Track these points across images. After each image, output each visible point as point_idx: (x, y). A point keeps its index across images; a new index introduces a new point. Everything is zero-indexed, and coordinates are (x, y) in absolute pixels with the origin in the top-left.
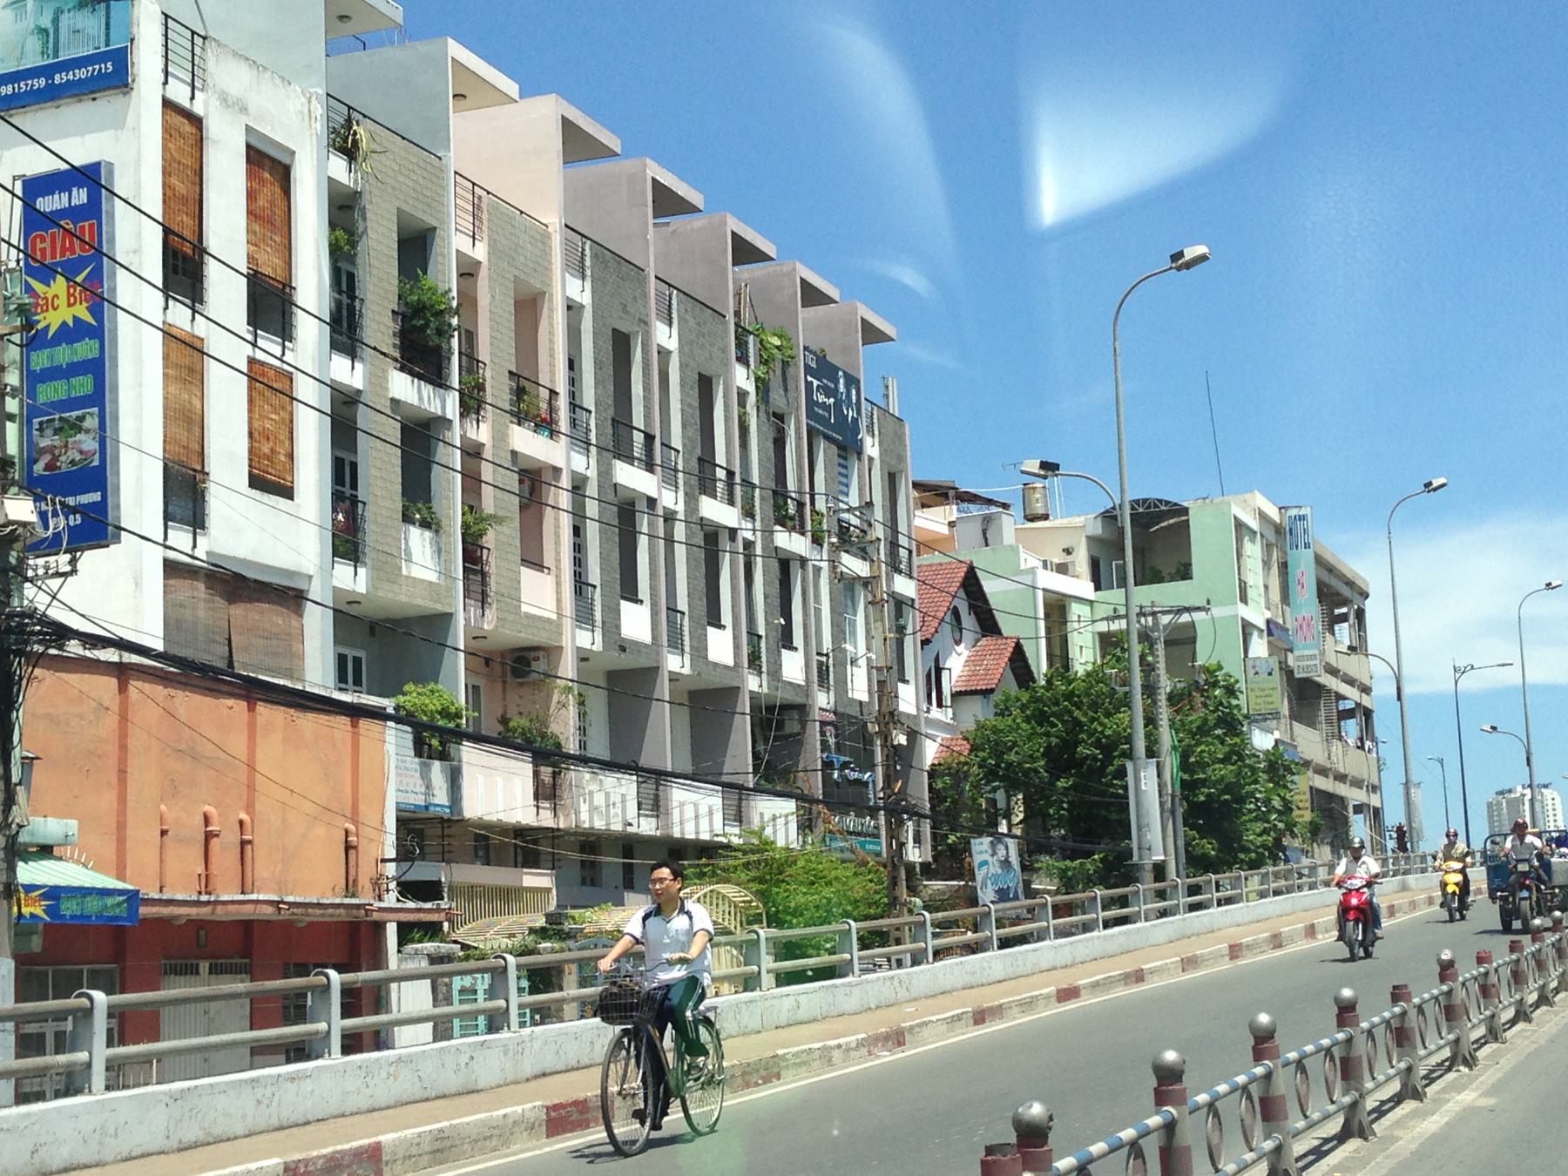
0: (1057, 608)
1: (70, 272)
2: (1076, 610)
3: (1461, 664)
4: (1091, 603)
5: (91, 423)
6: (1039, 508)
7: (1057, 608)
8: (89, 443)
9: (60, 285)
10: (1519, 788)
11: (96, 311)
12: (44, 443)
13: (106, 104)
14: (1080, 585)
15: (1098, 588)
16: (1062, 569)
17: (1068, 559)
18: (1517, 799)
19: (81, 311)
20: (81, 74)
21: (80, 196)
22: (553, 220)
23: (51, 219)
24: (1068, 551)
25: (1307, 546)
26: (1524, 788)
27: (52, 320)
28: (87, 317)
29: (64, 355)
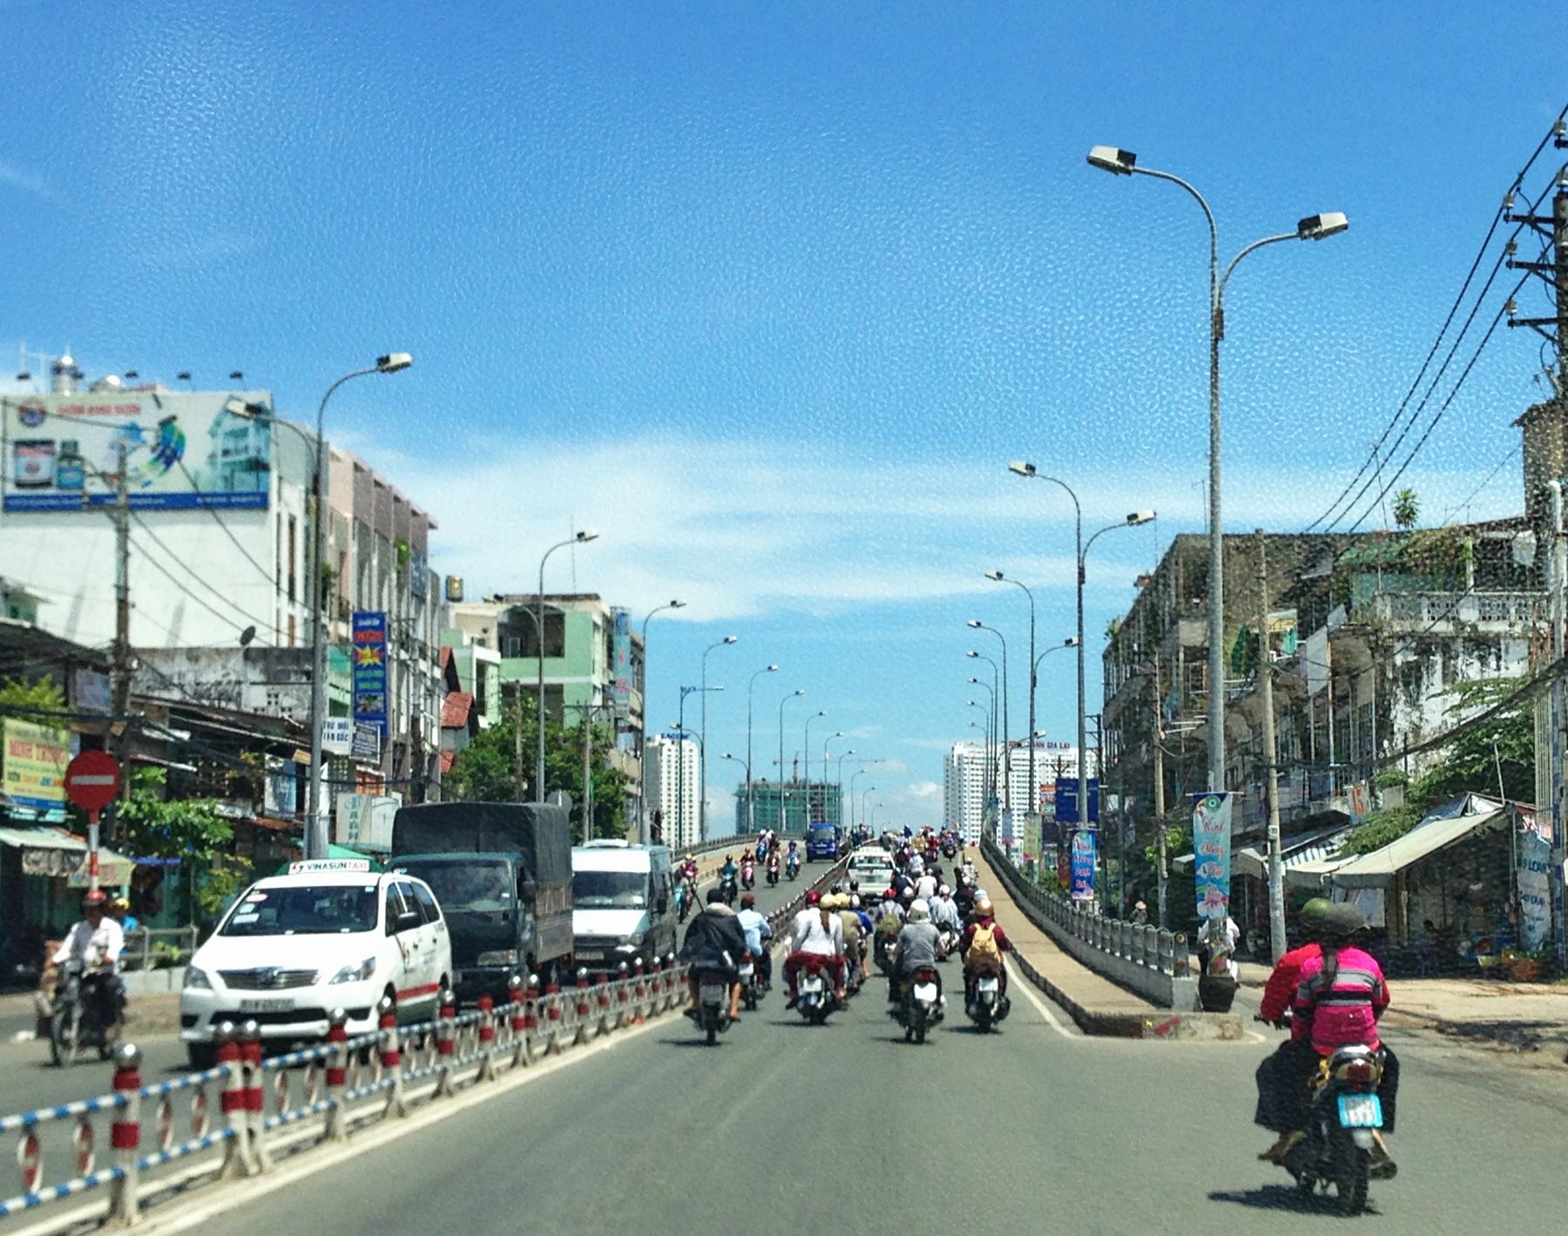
0: (482, 667)
1: (372, 646)
2: (491, 671)
3: (686, 685)
4: (498, 666)
5: (381, 698)
6: (457, 594)
7: (482, 667)
8: (380, 705)
9: (367, 650)
10: (658, 738)
11: (383, 661)
12: (362, 702)
13: (255, 515)
14: (491, 654)
15: (502, 657)
16: (482, 643)
17: (485, 636)
18: (655, 749)
19: (377, 661)
20: (244, 500)
21: (376, 622)
22: (349, 515)
23: (364, 628)
24: (485, 631)
25: (627, 633)
26: (663, 737)
27: (366, 662)
28: (379, 663)
29: (369, 674)
